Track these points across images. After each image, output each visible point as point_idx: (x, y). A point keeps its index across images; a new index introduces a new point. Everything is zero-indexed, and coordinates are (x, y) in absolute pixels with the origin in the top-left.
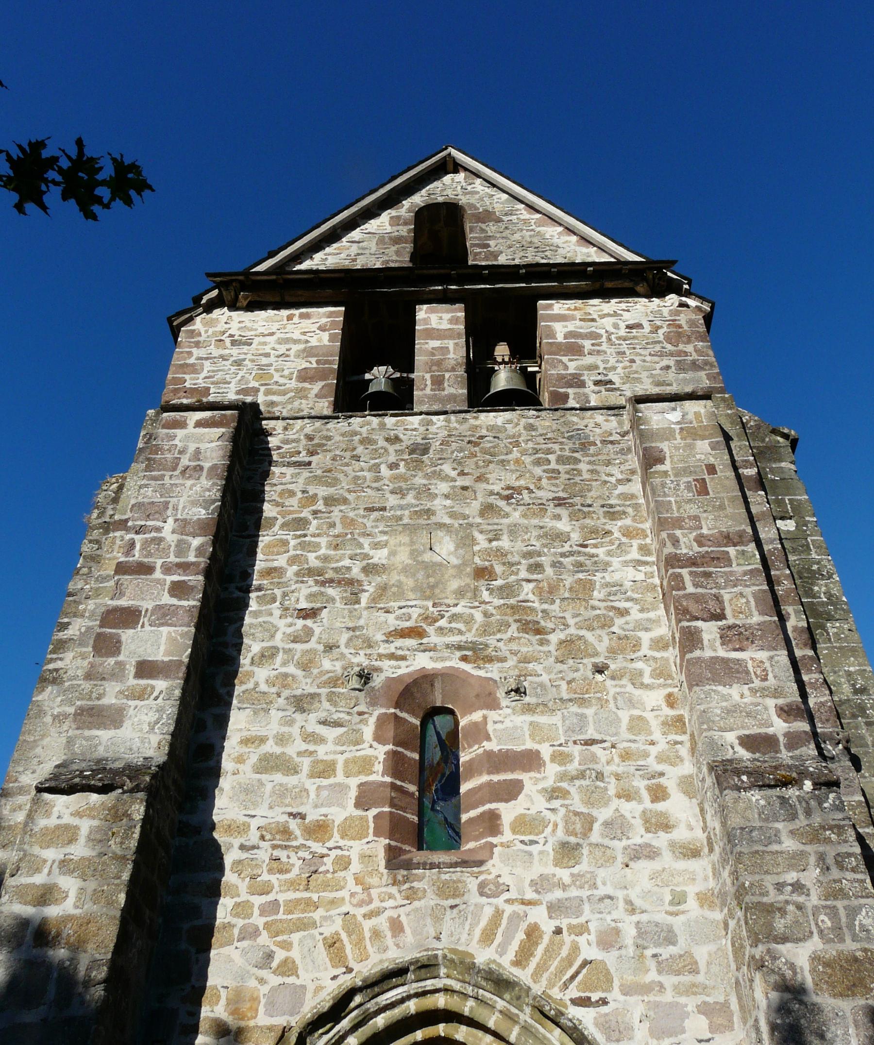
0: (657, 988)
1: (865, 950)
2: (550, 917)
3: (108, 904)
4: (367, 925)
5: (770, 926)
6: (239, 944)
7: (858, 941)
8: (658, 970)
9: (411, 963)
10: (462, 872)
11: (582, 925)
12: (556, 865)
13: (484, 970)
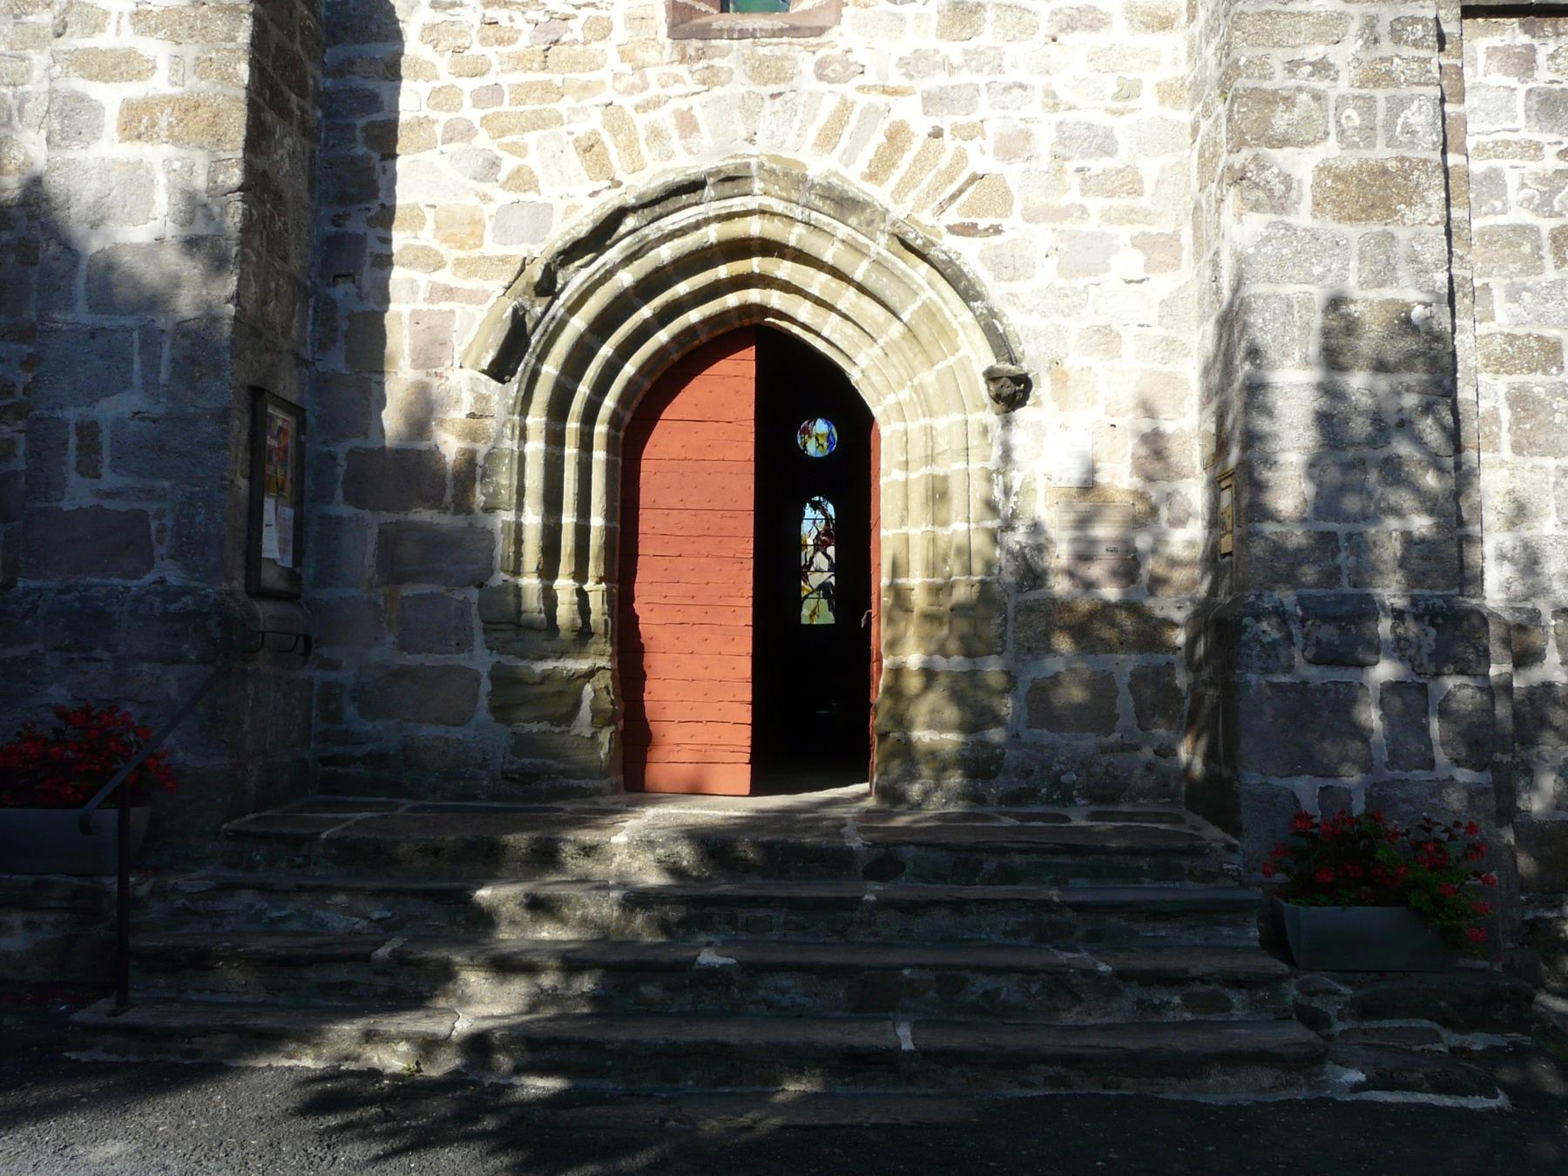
0: (1078, 214)
1: (1402, 159)
2: (926, 113)
3: (223, 79)
4: (641, 121)
5: (1265, 123)
6: (446, 148)
7: (1395, 147)
8: (1082, 190)
9: (710, 174)
10: (790, 44)
11: (974, 126)
12: (941, 37)
13: (820, 185)
